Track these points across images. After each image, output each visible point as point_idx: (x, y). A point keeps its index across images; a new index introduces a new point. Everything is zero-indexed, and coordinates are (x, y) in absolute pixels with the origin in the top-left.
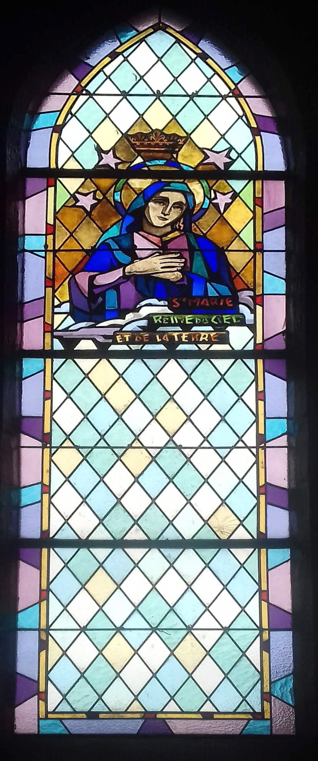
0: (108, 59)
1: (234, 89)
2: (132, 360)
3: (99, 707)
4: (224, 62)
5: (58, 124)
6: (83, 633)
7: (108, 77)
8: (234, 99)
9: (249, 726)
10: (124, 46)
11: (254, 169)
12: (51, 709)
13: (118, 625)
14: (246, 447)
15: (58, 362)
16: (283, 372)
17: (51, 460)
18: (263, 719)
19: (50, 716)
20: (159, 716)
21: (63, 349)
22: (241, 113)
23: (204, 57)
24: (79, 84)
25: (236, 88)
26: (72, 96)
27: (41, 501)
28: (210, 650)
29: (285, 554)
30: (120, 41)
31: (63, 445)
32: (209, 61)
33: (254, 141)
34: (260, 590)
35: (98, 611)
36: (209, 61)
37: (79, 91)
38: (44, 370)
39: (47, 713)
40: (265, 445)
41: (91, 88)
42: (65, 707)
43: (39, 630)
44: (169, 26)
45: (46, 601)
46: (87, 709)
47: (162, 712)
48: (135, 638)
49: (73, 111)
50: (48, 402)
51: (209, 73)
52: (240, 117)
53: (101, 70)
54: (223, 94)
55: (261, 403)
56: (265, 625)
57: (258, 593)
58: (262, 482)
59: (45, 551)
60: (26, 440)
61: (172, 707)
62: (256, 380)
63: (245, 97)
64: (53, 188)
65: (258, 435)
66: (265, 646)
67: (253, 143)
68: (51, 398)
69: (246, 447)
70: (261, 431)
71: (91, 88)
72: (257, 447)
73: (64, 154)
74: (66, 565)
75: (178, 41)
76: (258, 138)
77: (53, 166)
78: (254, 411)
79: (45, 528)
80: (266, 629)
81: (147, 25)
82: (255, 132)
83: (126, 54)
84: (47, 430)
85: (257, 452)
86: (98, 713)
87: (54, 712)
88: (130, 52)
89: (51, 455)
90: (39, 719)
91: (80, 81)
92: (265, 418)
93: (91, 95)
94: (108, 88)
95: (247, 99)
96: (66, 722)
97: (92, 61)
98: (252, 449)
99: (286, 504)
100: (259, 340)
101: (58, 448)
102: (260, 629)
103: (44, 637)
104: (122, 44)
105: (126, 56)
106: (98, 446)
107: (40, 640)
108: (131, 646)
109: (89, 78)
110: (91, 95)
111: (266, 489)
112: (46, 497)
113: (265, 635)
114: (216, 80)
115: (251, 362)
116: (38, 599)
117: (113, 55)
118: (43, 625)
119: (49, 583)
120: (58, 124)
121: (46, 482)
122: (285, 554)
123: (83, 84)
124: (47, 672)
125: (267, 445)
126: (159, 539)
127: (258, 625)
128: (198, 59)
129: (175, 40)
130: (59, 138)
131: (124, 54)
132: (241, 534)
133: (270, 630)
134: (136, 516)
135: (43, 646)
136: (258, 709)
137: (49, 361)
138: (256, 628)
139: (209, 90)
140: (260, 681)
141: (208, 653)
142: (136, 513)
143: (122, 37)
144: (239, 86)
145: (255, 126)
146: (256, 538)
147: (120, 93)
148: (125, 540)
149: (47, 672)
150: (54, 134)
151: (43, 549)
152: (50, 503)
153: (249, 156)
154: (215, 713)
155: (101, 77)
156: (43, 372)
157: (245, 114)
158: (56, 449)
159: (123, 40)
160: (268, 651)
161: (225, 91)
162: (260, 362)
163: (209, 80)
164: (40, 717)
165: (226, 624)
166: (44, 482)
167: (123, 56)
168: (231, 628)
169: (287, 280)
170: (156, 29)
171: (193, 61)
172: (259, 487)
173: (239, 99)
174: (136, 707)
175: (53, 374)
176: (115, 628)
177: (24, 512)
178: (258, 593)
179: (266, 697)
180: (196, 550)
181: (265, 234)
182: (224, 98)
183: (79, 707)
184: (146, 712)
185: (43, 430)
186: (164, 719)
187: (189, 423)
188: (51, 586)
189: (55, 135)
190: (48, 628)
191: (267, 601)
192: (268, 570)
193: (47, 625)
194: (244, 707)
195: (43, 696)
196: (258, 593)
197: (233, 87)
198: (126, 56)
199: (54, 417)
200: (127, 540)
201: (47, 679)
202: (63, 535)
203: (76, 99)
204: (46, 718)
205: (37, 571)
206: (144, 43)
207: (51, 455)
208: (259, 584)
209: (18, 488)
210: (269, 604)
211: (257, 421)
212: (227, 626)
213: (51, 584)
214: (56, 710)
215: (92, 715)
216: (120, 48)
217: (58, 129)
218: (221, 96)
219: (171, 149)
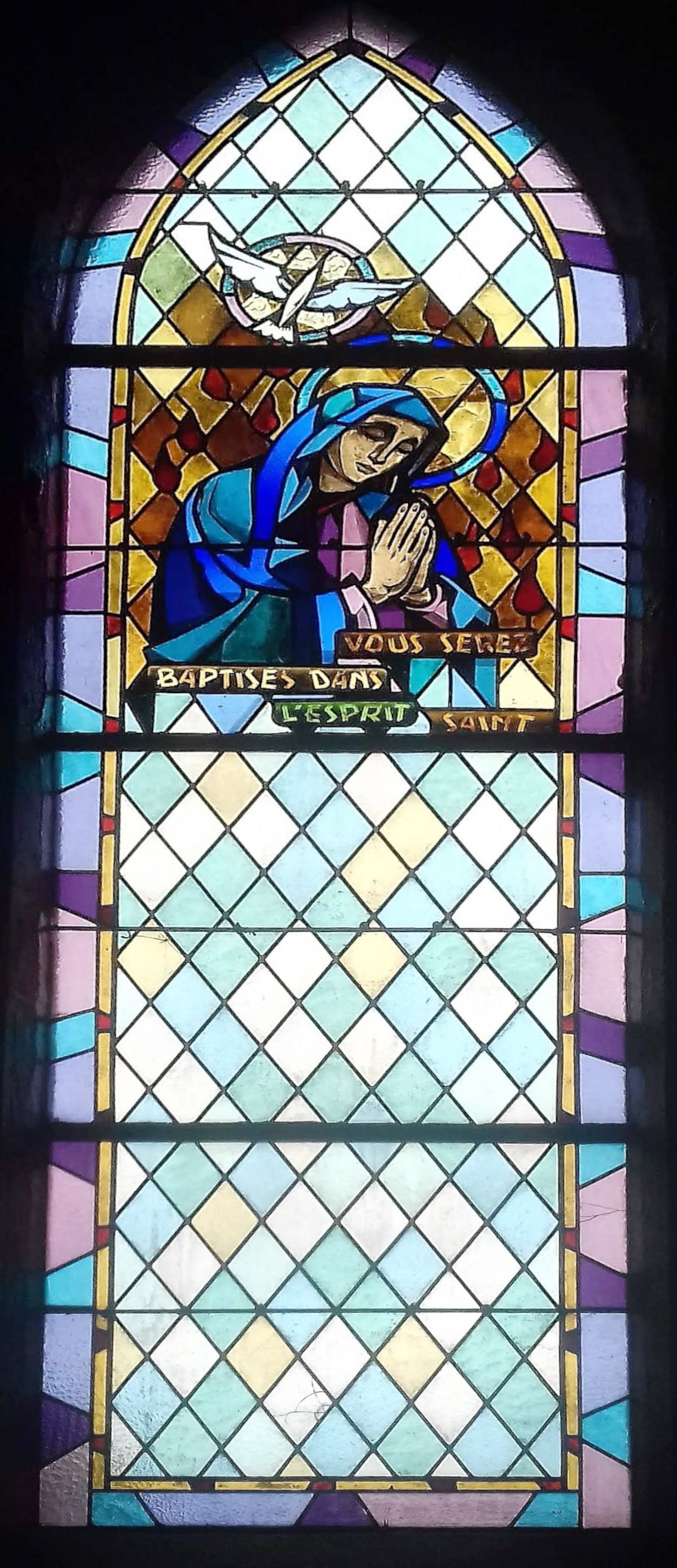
1: (514, 177)
2: (289, 754)
4: (492, 119)
7: (244, 153)
10: (273, 89)
11: (556, 343)
12: (115, 1472)
15: (130, 758)
16: (618, 779)
17: (116, 965)
18: (564, 1489)
20: (340, 1486)
21: (140, 731)
22: (529, 229)
23: (449, 110)
24: (179, 174)
25: (518, 175)
26: (166, 196)
27: (95, 1049)
29: (616, 1154)
30: (267, 82)
32: (458, 118)
33: (557, 288)
34: (561, 1228)
36: (458, 118)
37: (179, 187)
38: (101, 774)
39: (108, 1478)
41: (207, 177)
42: (145, 1467)
44: (370, 48)
46: (196, 1474)
47: (351, 1478)
48: (299, 1328)
51: (458, 140)
52: (528, 237)
53: (231, 139)
54: (489, 186)
56: (571, 1302)
57: (557, 1234)
58: (568, 1010)
59: (105, 1147)
61: (373, 1467)
62: (559, 793)
63: (533, 191)
65: (561, 909)
66: (571, 1342)
67: (554, 292)
68: (116, 832)
71: (207, 177)
72: (558, 932)
74: (150, 1176)
75: (393, 78)
76: (564, 282)
78: (555, 861)
80: (572, 1311)
81: (38, 984)
82: (560, 269)
83: (281, 104)
84: (107, 899)
86: (214, 1479)
87: (122, 1478)
89: (117, 952)
90: (91, 1491)
92: (577, 873)
93: (204, 192)
95: (539, 195)
96: (150, 1499)
97: (207, 125)
99: (621, 1055)
103: (103, 1324)
104: (270, 86)
107: (96, 1332)
109: (284, 86)
110: (204, 192)
112: (105, 1038)
113: (571, 1324)
114: (471, 155)
115: (549, 760)
116: (91, 1247)
117: (253, 111)
118: (102, 1304)
119: (114, 1215)
122: (616, 1154)
124: (110, 1396)
125: (584, 927)
128: (433, 111)
129: (383, 75)
130: (137, 285)
132: (522, 1114)
133: (580, 1309)
134: (297, 1078)
135: (102, 1341)
136: (555, 1472)
137: (111, 757)
142: (298, 1072)
143: (270, 74)
144: (520, 169)
145: (561, 257)
147: (266, 187)
150: (126, 276)
151: (102, 1144)
152: (114, 1053)
153: (547, 320)
155: (230, 153)
156: (99, 778)
157: (537, 230)
159: (272, 79)
160: (577, 1350)
161: (493, 180)
162: (569, 758)
163: (457, 156)
165: (487, 1300)
166: (101, 1008)
167: (275, 109)
169: (628, 584)
170: (342, 50)
172: (560, 1018)
173: (523, 195)
174: (298, 1468)
175: (120, 781)
177: (62, 1071)
178: (557, 1234)
179: (572, 1445)
181: (582, 485)
182: (494, 194)
184: (319, 1477)
185: (100, 902)
186: (354, 1493)
187: (412, 884)
188: (119, 1221)
189: (130, 279)
190: (110, 1313)
191: (576, 1249)
193: (111, 1300)
194: (526, 1468)
195: (103, 1444)
196: (557, 1234)
197: (510, 173)
201: (110, 1408)
202: (138, 1117)
203: (175, 202)
204: (107, 1489)
207: (117, 952)
209: (50, 1020)
210: (581, 1258)
211: (559, 880)
212: (490, 1303)
215: (202, 1484)
216: (265, 96)
217: (134, 267)
218: (484, 189)
219: (410, 472)
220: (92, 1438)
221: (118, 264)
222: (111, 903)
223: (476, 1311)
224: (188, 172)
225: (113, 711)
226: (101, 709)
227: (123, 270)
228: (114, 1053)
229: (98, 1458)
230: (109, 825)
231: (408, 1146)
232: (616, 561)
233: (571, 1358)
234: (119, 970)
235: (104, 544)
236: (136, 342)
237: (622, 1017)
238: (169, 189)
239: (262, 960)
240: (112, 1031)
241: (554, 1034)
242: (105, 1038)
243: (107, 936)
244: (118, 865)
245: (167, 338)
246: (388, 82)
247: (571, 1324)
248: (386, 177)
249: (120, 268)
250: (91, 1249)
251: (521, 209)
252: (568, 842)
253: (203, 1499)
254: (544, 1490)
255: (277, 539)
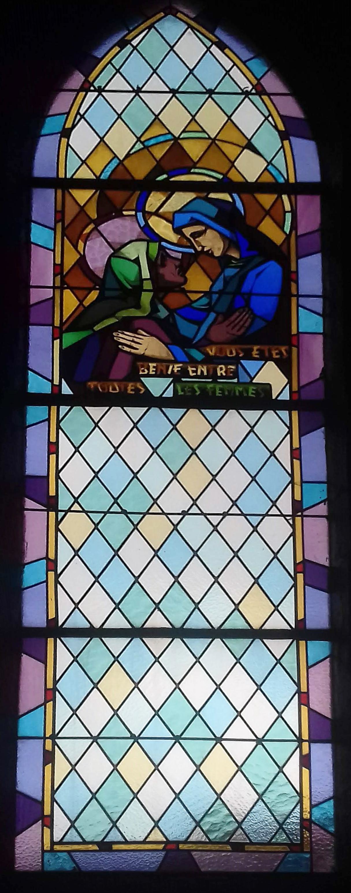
0: (117, 49)
3: (114, 836)
4: (246, 55)
5: (66, 127)
6: (218, 744)
7: (118, 71)
8: (257, 97)
9: (159, 861)
13: (95, 734)
14: (282, 515)
15: (64, 409)
17: (57, 530)
19: (56, 847)
21: (72, 393)
22: (267, 114)
23: (222, 46)
24: (86, 81)
25: (259, 83)
27: (46, 581)
28: (242, 765)
31: (160, 512)
33: (283, 147)
35: (153, 717)
36: (227, 51)
37: (86, 87)
38: (49, 420)
39: (53, 843)
40: (302, 514)
42: (73, 836)
43: (45, 738)
45: (52, 702)
46: (99, 839)
47: (186, 842)
49: (82, 112)
50: (53, 457)
51: (228, 64)
52: (266, 118)
55: (296, 462)
58: (299, 559)
59: (51, 641)
60: (29, 503)
61: (198, 836)
63: (269, 95)
64: (293, 390)
69: (282, 515)
70: (298, 497)
72: (294, 516)
73: (73, 163)
77: (62, 175)
79: (52, 616)
82: (284, 136)
83: (135, 43)
84: (52, 493)
85: (294, 521)
87: (61, 842)
88: (140, 39)
90: (43, 851)
91: (87, 76)
94: (118, 83)
98: (288, 518)
100: (295, 388)
101: (66, 512)
102: (300, 740)
104: (130, 31)
105: (135, 45)
106: (279, 513)
107: (45, 752)
108: (234, 762)
111: (304, 567)
113: (305, 745)
115: (284, 414)
117: (123, 44)
118: (49, 733)
119: (56, 682)
120: (66, 127)
121: (52, 556)
123: (91, 79)
124: (54, 792)
125: (305, 513)
126: (63, 627)
127: (297, 734)
128: (214, 46)
131: (132, 43)
133: (311, 741)
138: (295, 739)
139: (227, 86)
140: (299, 804)
141: (239, 769)
146: (294, 626)
148: (64, 628)
149: (54, 792)
152: (57, 582)
154: (247, 843)
156: (47, 422)
157: (270, 115)
158: (64, 513)
162: (295, 414)
164: (45, 848)
168: (223, 737)
171: (208, 49)
173: (263, 97)
174: (157, 836)
175: (59, 422)
176: (173, 737)
177: (27, 595)
180: (224, 639)
182: (246, 94)
183: (89, 836)
184: (168, 842)
186: (189, 851)
190: (54, 737)
192: (308, 668)
196: (297, 695)
197: (255, 82)
198: (135, 45)
199: (60, 527)
200: (66, 628)
205: (42, 665)
206: (153, 30)
207: (58, 523)
208: (298, 684)
213: (57, 683)
214: (65, 840)
217: (66, 133)
220: (43, 817)
221: (57, 133)
222: (54, 495)
223: (253, 740)
224: (57, 323)
225: (56, 382)
226: (51, 379)
227: (61, 136)
228: (57, 582)
229: (47, 831)
230: (53, 449)
231: (191, 410)
232: (318, 304)
233: (305, 771)
234: (55, 804)
235: (52, 285)
236: (69, 176)
237: (327, 564)
238: (82, 89)
239: (136, 527)
240: (56, 571)
241: (292, 574)
242: (51, 574)
243: (52, 514)
244: (58, 472)
245: (85, 174)
246: (189, 30)
247: (305, 751)
248: (155, 84)
249: (59, 135)
250: (43, 702)
251: (264, 106)
252: (296, 462)
253: (105, 855)
254: (292, 851)
255: (142, 392)
